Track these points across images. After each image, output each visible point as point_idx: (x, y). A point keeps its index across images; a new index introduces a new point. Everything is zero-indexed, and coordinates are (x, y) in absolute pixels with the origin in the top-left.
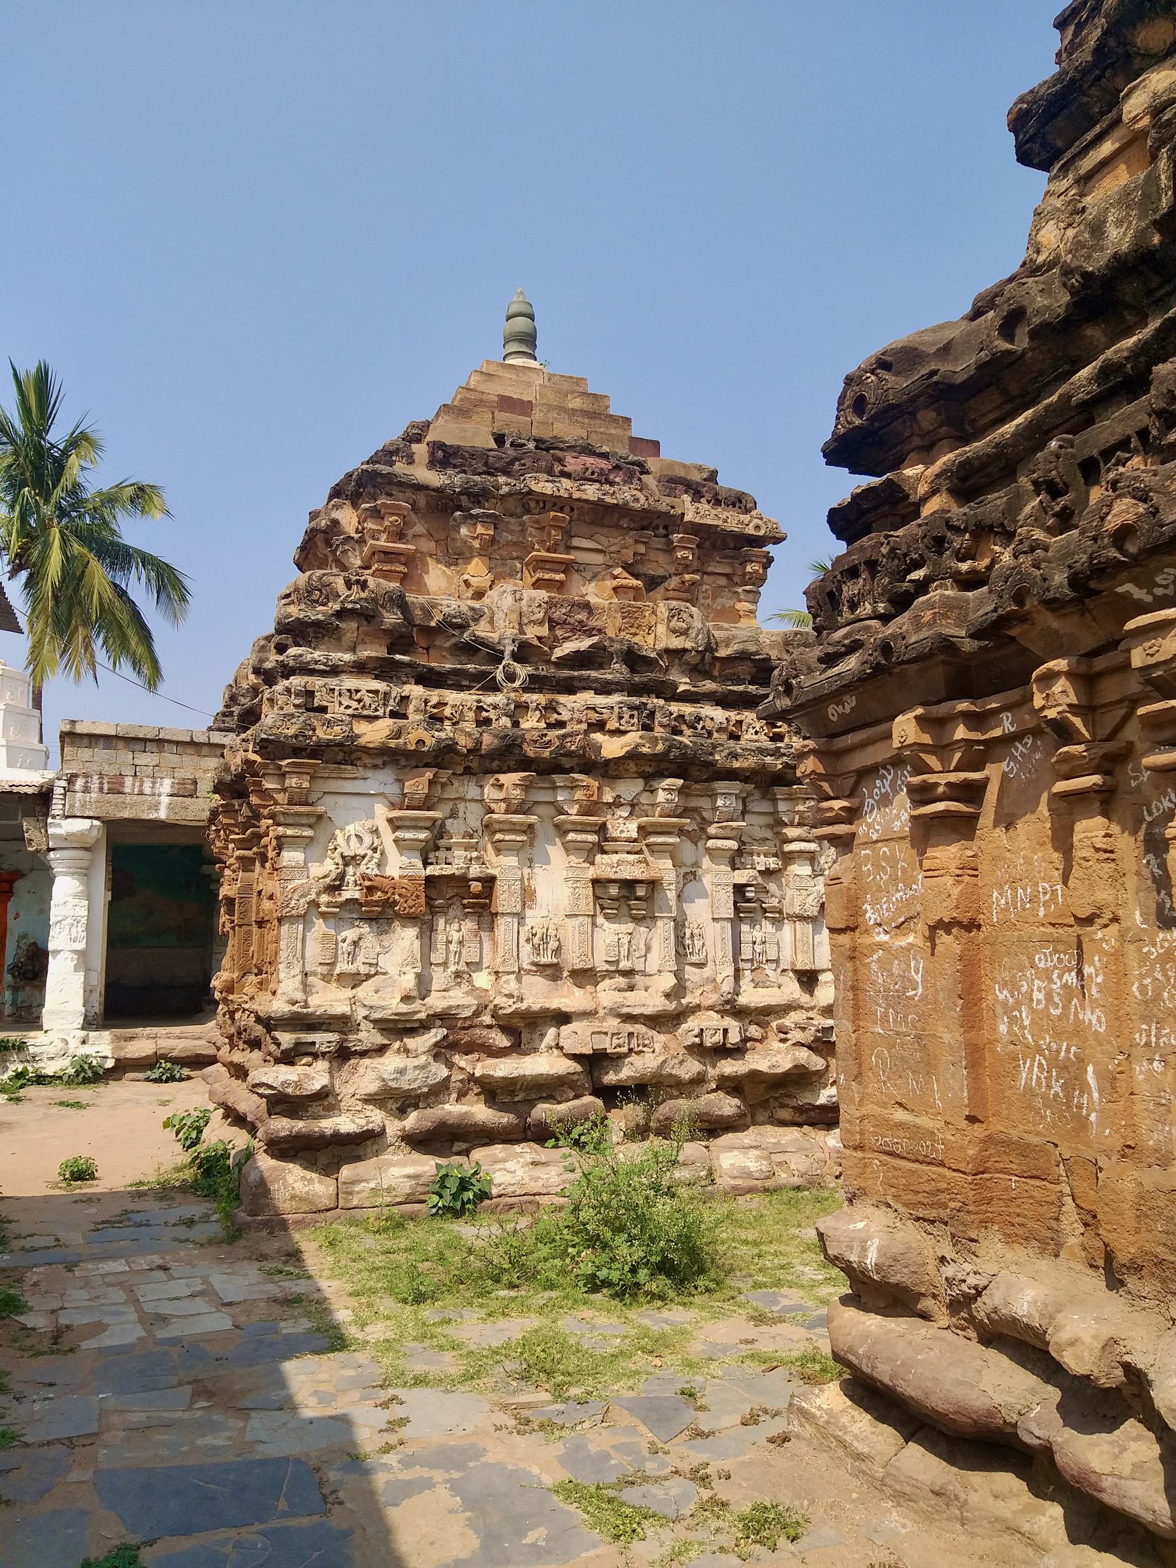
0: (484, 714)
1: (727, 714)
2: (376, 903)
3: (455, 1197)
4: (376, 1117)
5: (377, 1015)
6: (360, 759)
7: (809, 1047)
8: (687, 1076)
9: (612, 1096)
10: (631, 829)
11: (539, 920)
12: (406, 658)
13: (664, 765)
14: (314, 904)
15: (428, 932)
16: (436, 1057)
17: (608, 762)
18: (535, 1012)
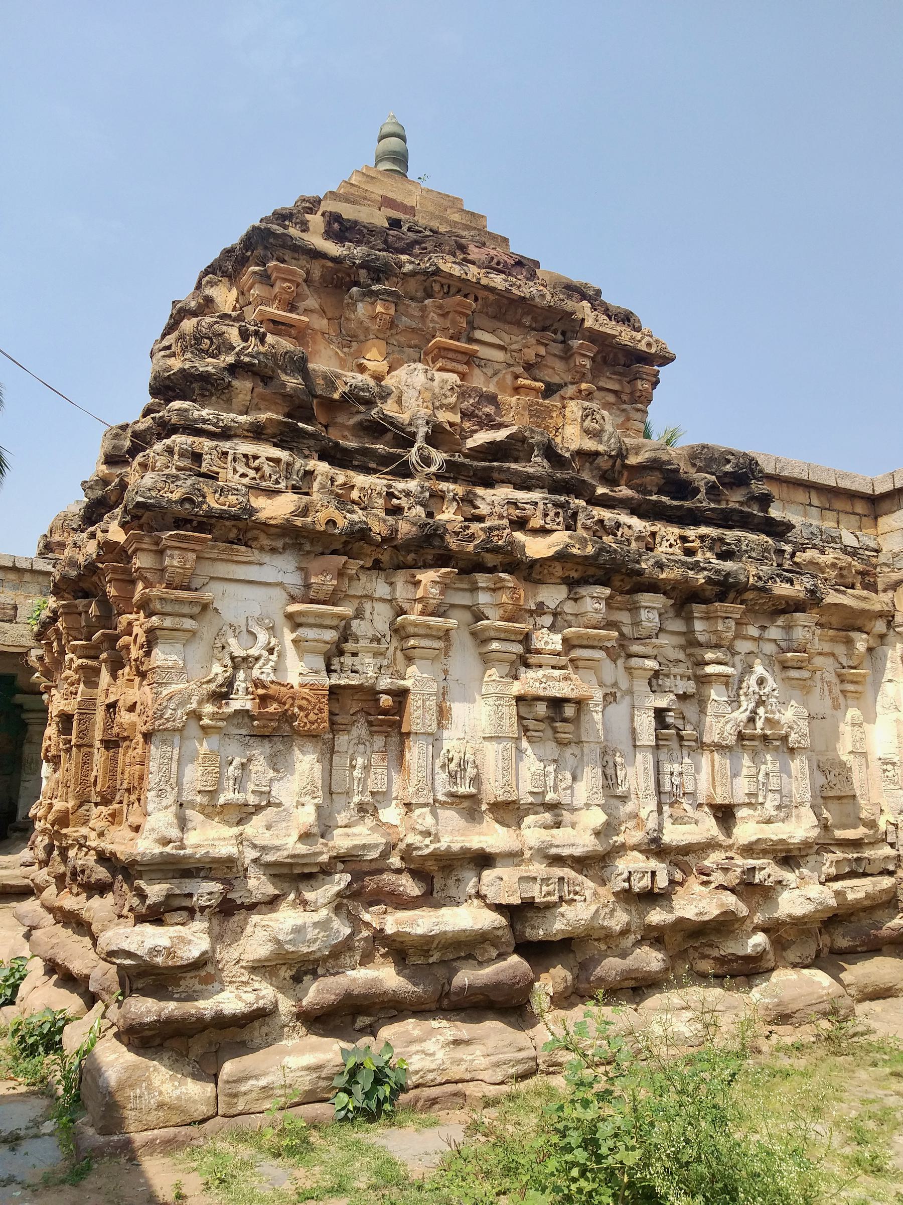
0: (395, 501)
1: (644, 524)
2: (271, 717)
3: (368, 1095)
4: (265, 992)
5: (269, 858)
6: (256, 539)
7: (733, 891)
8: (618, 928)
9: (540, 953)
10: (555, 641)
11: (455, 743)
12: (310, 428)
13: (591, 571)
14: (196, 716)
15: (330, 752)
16: (337, 909)
17: (534, 562)
18: (455, 854)
